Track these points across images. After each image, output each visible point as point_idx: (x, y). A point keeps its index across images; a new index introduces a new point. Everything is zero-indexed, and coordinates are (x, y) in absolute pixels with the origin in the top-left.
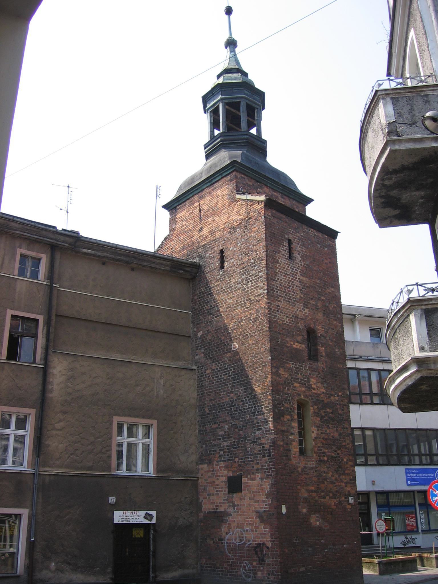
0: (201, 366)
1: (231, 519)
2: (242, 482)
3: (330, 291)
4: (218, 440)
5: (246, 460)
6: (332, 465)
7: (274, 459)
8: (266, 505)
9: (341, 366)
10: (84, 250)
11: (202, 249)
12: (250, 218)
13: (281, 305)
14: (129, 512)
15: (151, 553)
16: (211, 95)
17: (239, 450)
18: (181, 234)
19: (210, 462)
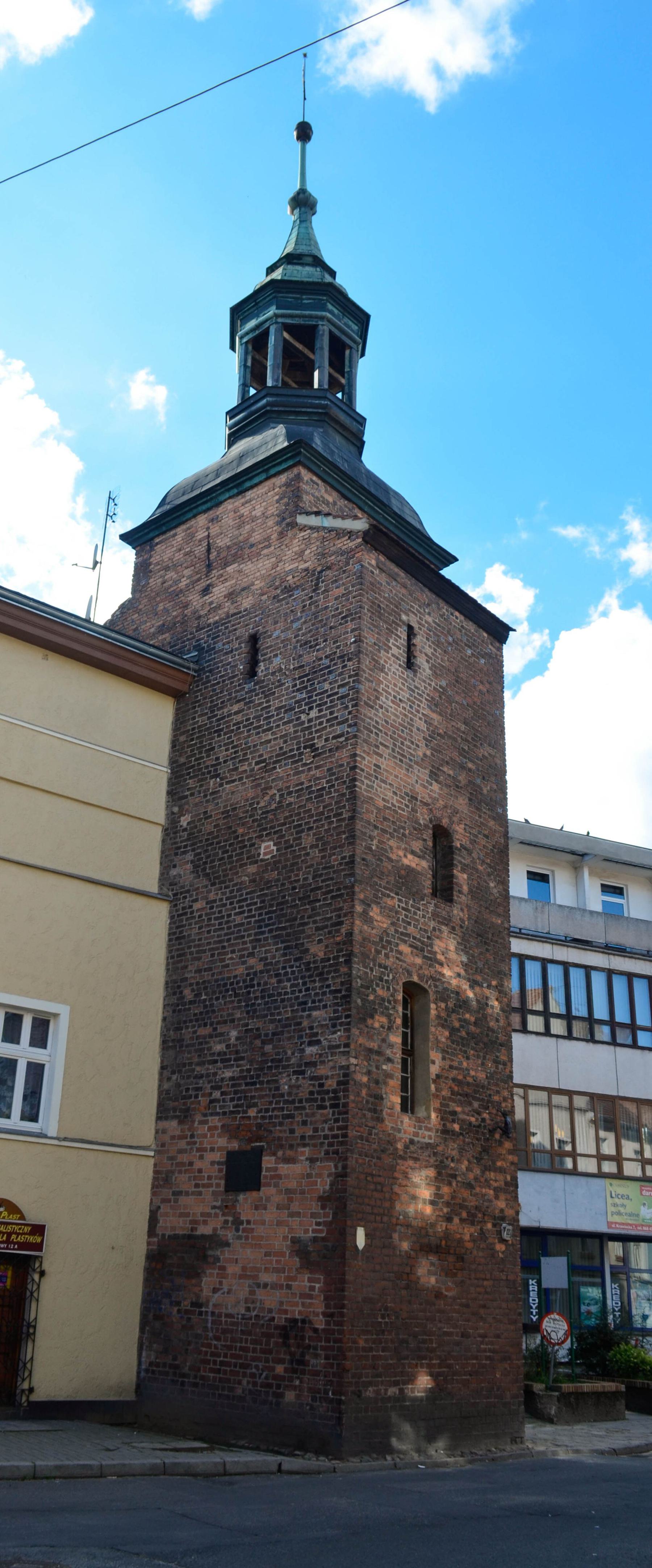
0: (181, 893)
1: (227, 1255)
3: (486, 754)
4: (209, 1064)
5: (276, 1113)
6: (468, 1144)
8: (318, 1224)
11: (207, 631)
13: (382, 763)
17: (261, 1089)
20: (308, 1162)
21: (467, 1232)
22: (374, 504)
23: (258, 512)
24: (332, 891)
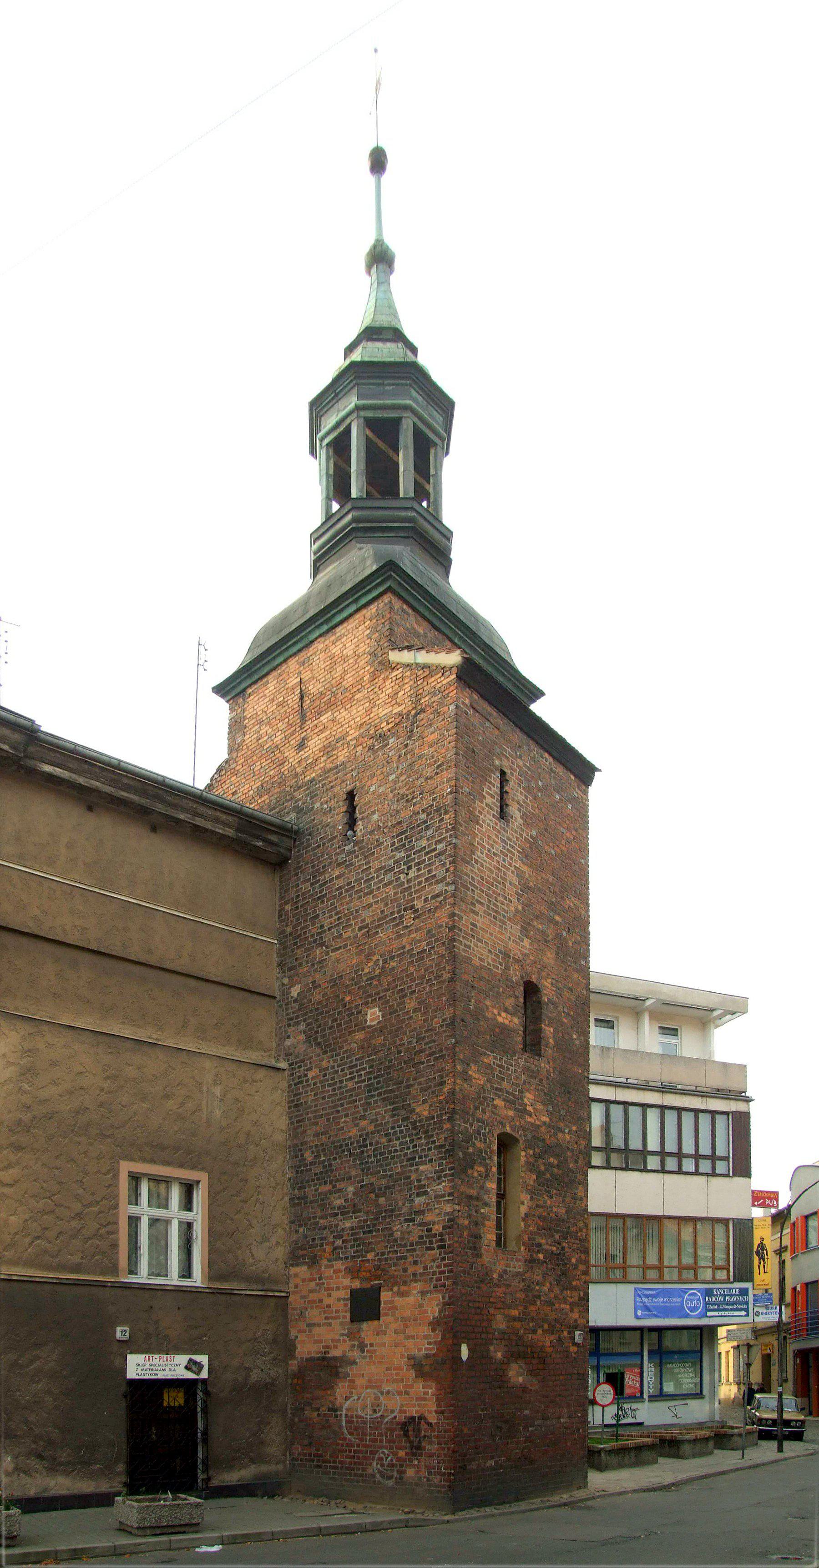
0: (297, 1063)
2: (382, 1299)
7: (451, 1252)
8: (429, 1343)
9: (580, 1071)
10: (47, 768)
11: (305, 791)
12: (422, 711)
14: (155, 1356)
15: (199, 1435)
16: (333, 399)
18: (255, 758)
19: (313, 1261)
20: (419, 1295)
23: (349, 652)
24: (435, 1053)
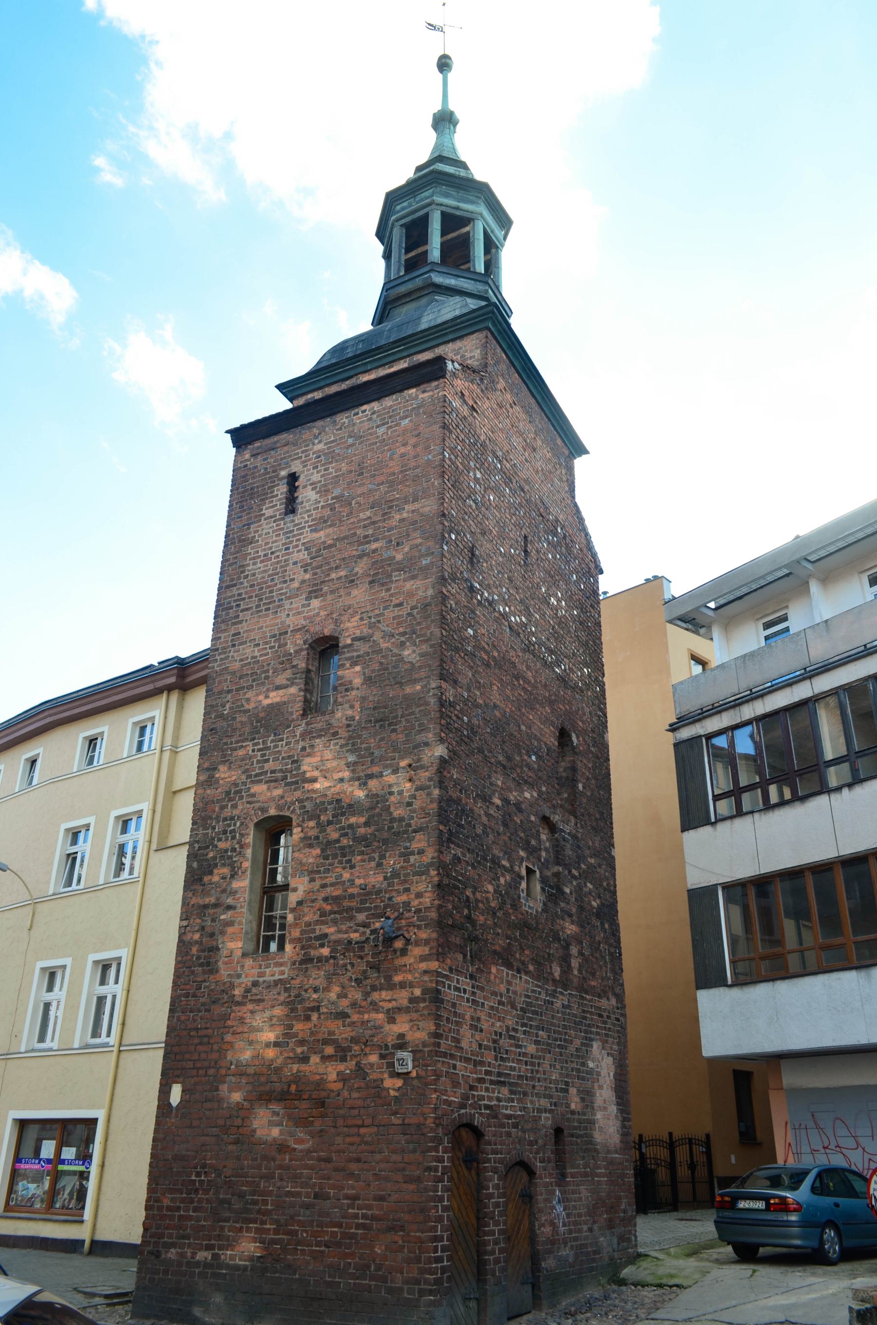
21: (332, 1072)
22: (372, 357)
